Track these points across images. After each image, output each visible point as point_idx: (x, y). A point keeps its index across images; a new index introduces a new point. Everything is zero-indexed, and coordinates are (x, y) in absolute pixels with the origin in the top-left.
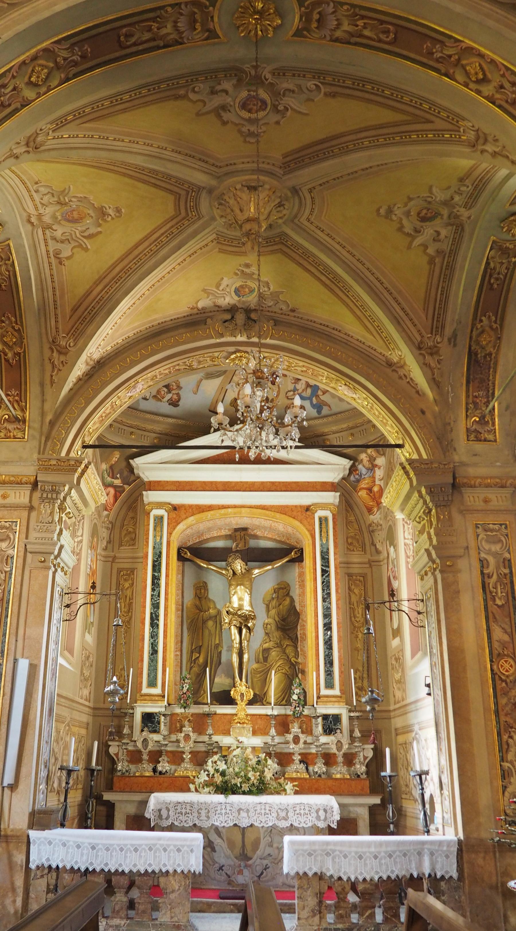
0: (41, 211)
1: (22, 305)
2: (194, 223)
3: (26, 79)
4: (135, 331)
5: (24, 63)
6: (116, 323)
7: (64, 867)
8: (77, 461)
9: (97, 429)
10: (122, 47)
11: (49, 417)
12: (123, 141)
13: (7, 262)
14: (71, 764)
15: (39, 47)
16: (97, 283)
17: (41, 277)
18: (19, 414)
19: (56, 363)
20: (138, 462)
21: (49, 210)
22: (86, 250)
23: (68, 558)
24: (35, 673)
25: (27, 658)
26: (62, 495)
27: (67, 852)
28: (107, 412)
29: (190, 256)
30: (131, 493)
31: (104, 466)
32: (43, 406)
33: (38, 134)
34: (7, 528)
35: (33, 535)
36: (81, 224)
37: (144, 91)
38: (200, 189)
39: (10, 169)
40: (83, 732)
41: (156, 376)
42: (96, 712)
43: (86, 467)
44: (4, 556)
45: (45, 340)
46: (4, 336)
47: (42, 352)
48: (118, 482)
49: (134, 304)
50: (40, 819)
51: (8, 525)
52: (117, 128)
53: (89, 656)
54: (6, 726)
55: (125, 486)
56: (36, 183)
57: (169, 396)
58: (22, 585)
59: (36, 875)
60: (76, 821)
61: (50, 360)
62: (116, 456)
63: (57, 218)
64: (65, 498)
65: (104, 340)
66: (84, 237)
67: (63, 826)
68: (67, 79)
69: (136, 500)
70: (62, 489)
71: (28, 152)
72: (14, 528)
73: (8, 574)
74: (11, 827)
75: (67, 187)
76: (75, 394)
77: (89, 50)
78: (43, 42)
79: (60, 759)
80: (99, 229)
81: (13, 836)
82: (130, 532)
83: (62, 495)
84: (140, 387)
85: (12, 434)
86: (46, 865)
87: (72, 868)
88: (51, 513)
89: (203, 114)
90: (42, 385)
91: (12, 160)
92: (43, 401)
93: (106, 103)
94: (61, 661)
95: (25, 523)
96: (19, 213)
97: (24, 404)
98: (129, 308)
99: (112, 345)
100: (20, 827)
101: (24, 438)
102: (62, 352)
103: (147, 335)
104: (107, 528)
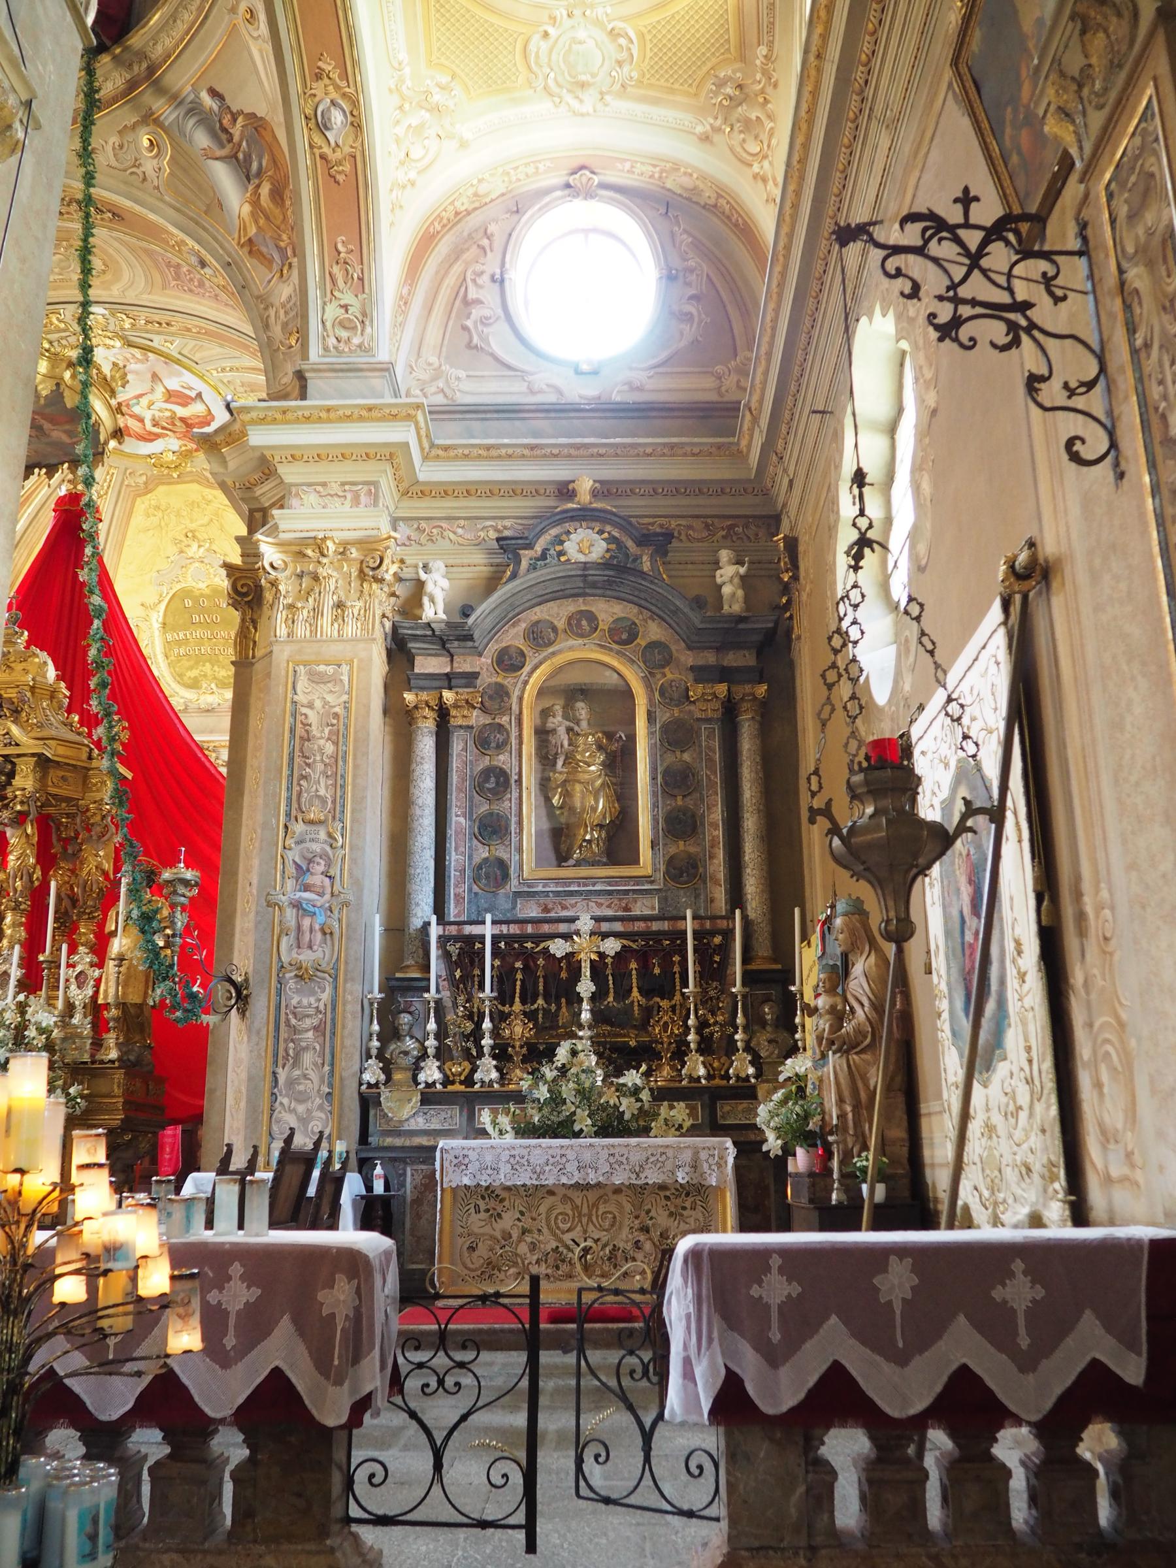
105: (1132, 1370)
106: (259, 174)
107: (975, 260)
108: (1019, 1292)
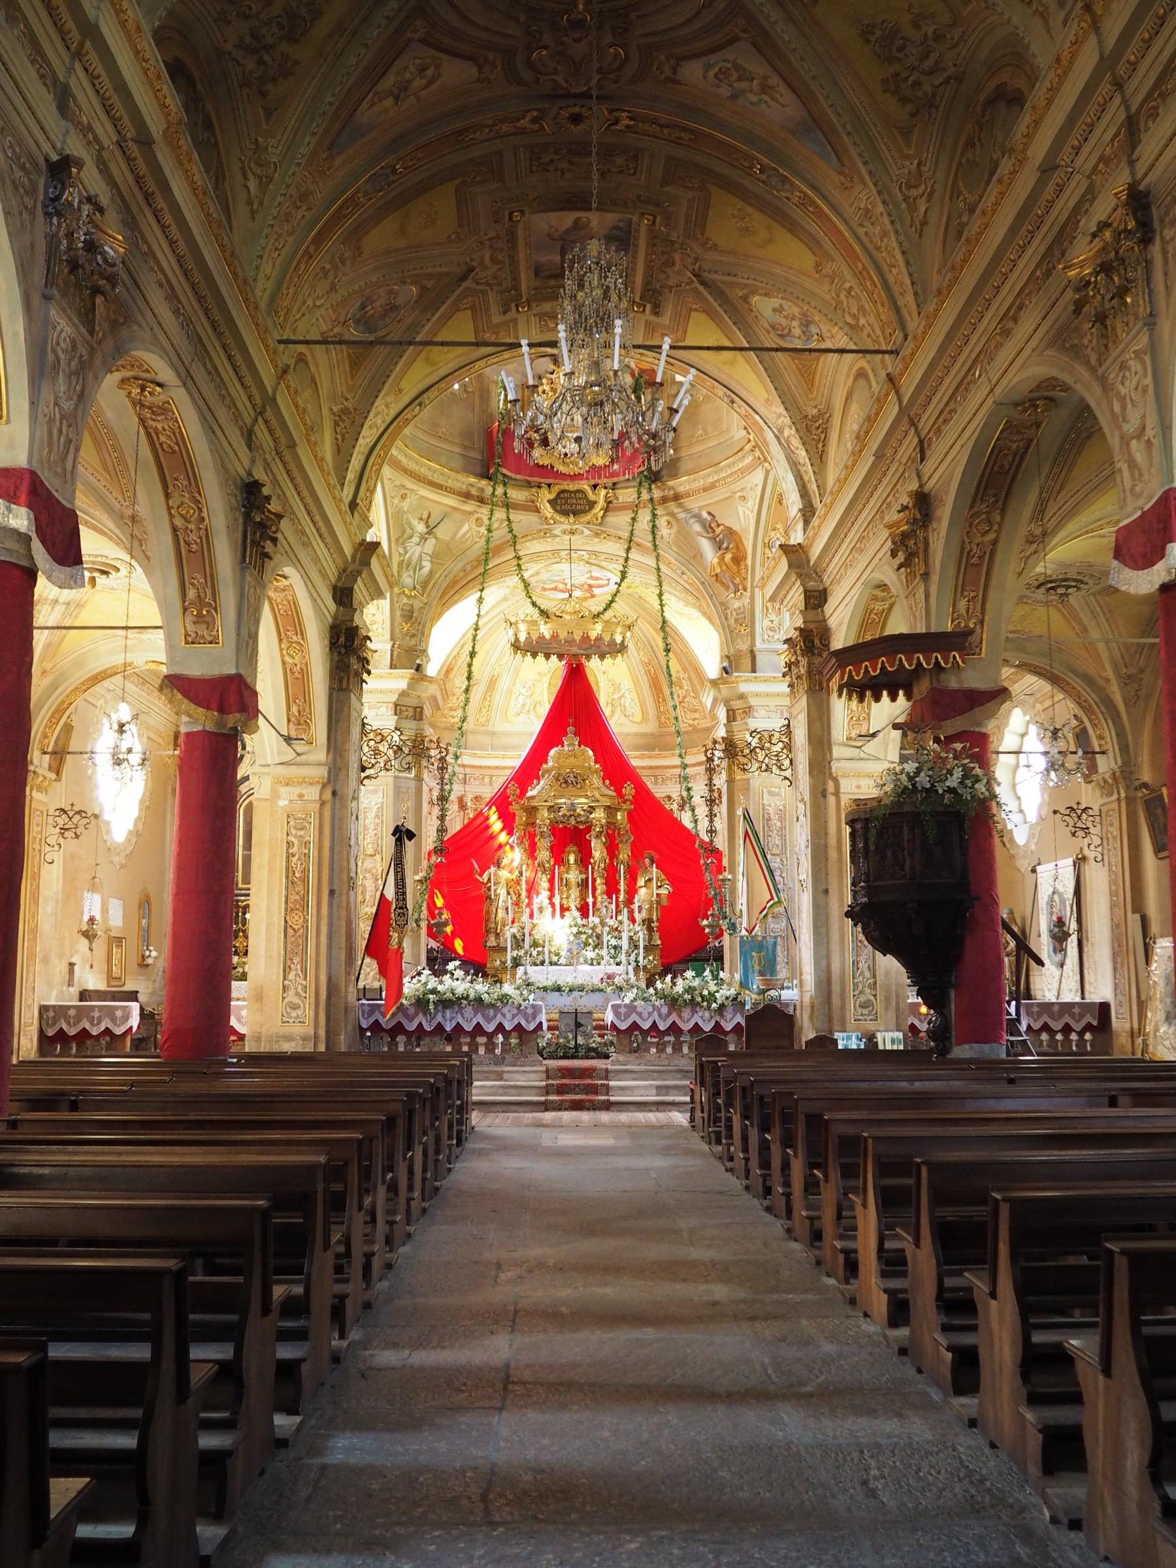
105: (1095, 1023)
106: (727, 548)
107: (1079, 817)
108: (1076, 1010)
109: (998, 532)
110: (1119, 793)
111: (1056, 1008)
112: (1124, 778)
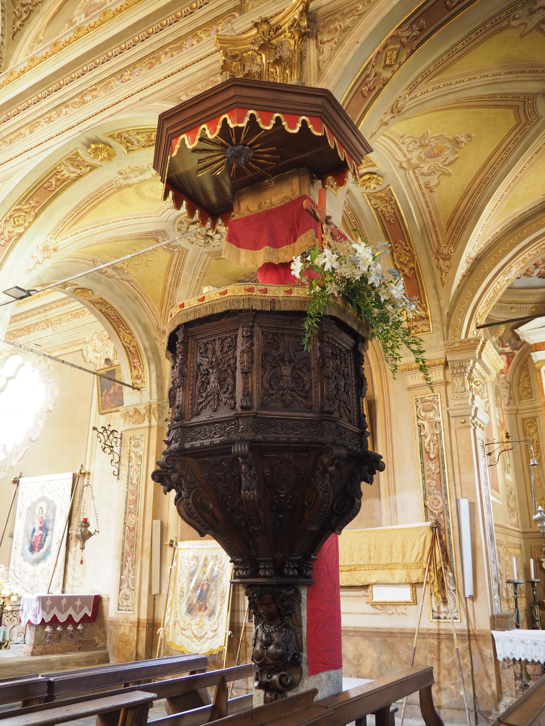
0: (409, 156)
1: (408, 231)
2: (534, 125)
3: (383, 65)
4: (501, 227)
5: (379, 53)
6: (484, 225)
7: (526, 660)
8: (476, 340)
9: (485, 311)
10: (449, 9)
11: (446, 311)
12: (463, 81)
13: (391, 202)
14: (516, 579)
15: (387, 37)
16: (462, 198)
17: (418, 206)
18: (422, 313)
19: (443, 268)
20: (522, 330)
21: (415, 154)
22: (449, 175)
23: (482, 416)
24: (474, 509)
25: (466, 498)
26: (469, 368)
27: (527, 648)
28: (491, 296)
29: (536, 153)
30: (521, 356)
31: (494, 339)
32: (440, 304)
33: (398, 101)
34: (431, 401)
35: (452, 403)
36: (441, 157)
37: (473, 36)
38: (534, 96)
39: (384, 135)
40: (518, 552)
41: (526, 258)
42: (525, 535)
43: (484, 343)
44: (433, 423)
45: (431, 253)
46: (399, 258)
47: (430, 263)
48: (508, 349)
49: (496, 205)
50: (499, 622)
51: (431, 399)
52: (456, 74)
53: (511, 491)
54: (459, 551)
55: (515, 351)
56: (402, 137)
57: (538, 271)
58: (451, 443)
59: (503, 666)
60: (525, 623)
61: (438, 267)
62: (502, 328)
63: (422, 158)
64: (471, 371)
65: (477, 240)
66: (445, 165)
67: (518, 627)
68: (413, 52)
69: (526, 361)
70: (467, 364)
71: (394, 117)
72: (436, 400)
73: (439, 436)
74: (477, 628)
75: (425, 132)
76: (462, 288)
77: (424, 23)
78: (389, 32)
79: (504, 574)
80: (457, 156)
81: (479, 635)
82: (526, 388)
83: (469, 368)
84: (514, 270)
85: (420, 330)
86: (511, 658)
87: (533, 661)
88: (462, 384)
89: (526, 34)
90: (435, 287)
91: (384, 127)
92: (439, 300)
93: (445, 57)
94: (492, 498)
95: (444, 395)
96: (394, 165)
97: (424, 305)
98: (493, 210)
99: (485, 242)
100: (485, 628)
101: (430, 331)
102: (446, 259)
103: (511, 228)
104: (507, 388)
109: (26, 229)
110: (150, 421)
111: (64, 602)
112: (159, 410)
